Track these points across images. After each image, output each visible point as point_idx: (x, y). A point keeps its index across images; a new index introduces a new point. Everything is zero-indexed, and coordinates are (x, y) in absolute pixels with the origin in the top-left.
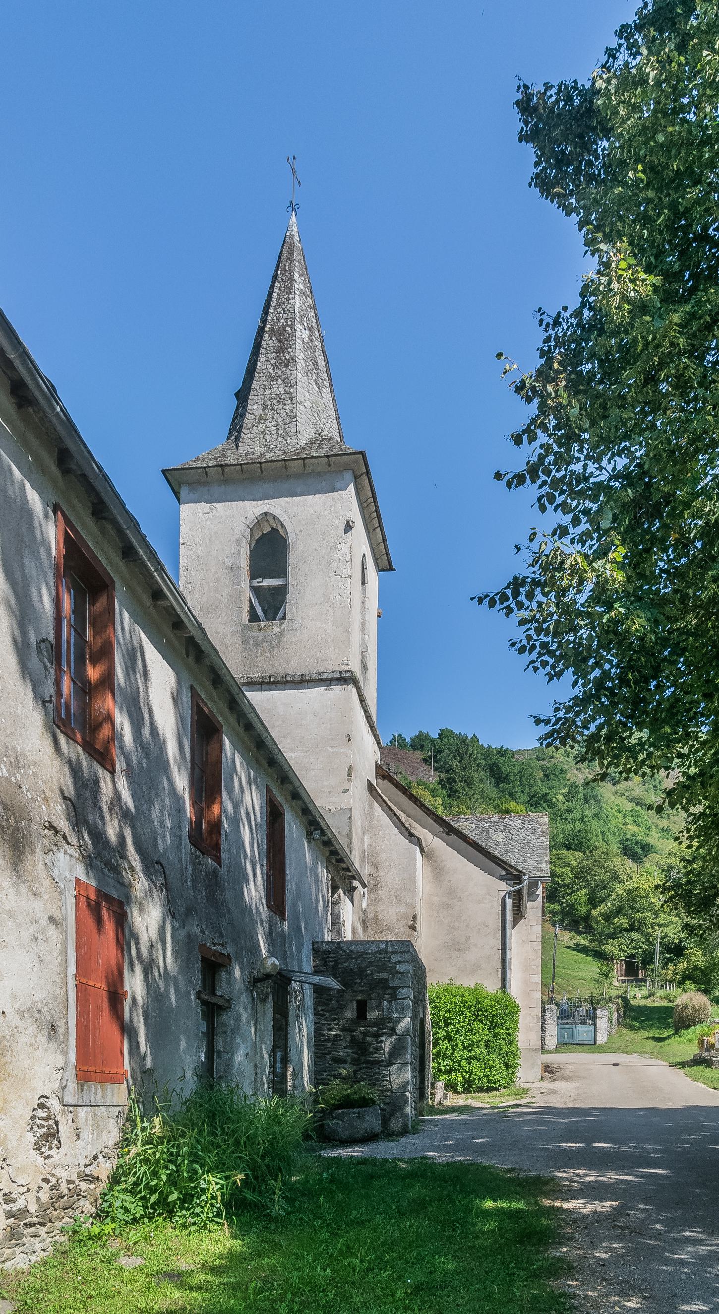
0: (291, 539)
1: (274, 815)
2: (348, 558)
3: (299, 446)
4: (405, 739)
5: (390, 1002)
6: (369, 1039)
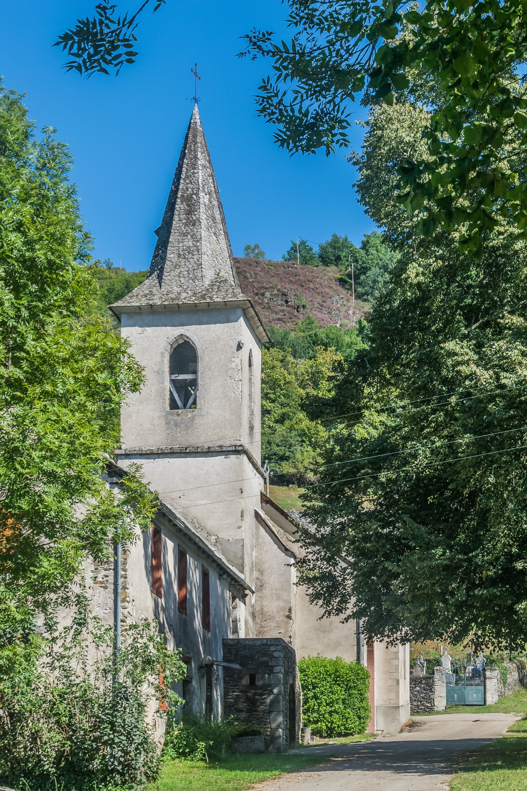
0: (199, 353)
1: (205, 576)
2: (240, 368)
3: (204, 288)
4: (311, 249)
5: (269, 675)
6: (257, 697)
